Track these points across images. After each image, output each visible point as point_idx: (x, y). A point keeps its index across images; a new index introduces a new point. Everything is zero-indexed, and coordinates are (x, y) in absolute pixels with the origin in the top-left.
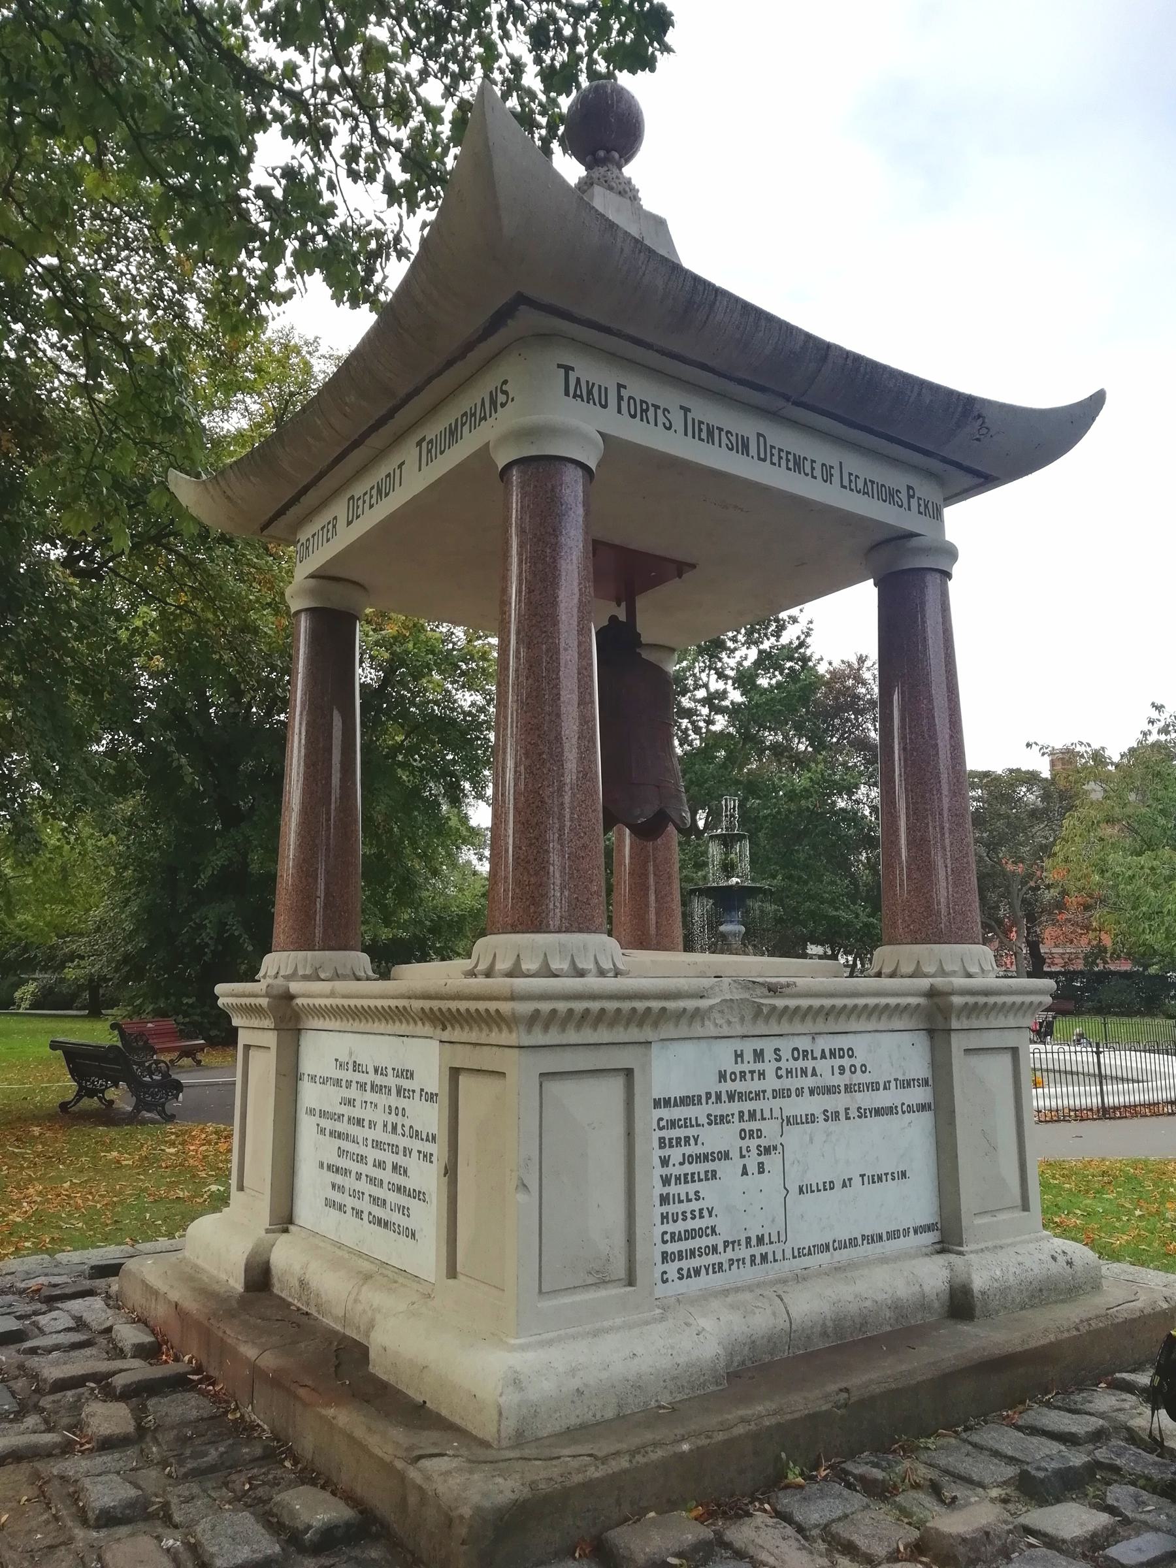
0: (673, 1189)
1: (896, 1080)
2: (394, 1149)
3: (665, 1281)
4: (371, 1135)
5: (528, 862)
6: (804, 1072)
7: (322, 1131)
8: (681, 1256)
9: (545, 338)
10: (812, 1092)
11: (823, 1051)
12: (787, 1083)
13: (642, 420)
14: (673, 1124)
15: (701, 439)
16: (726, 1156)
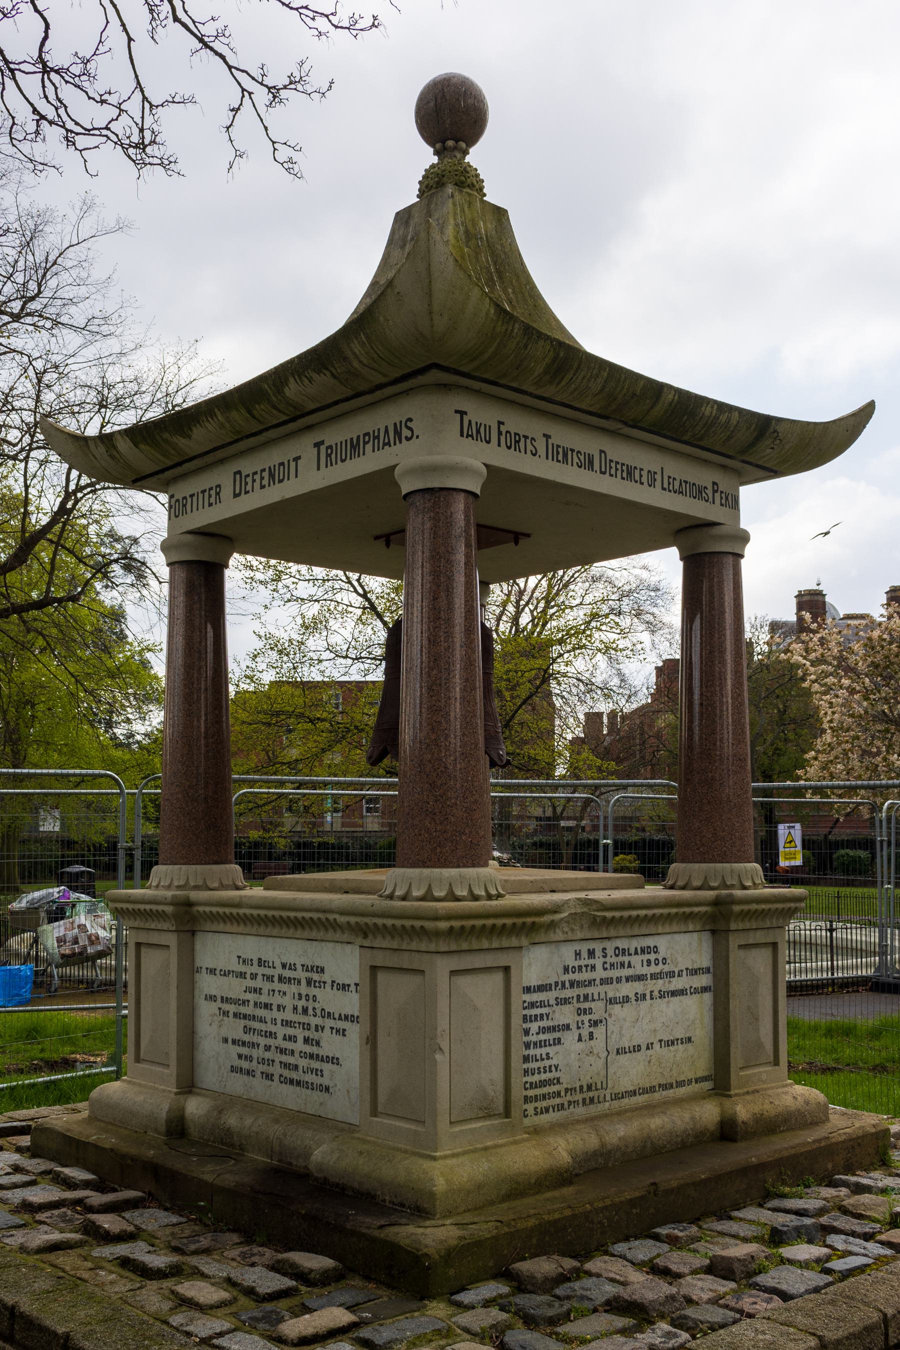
0: (532, 1052)
1: (687, 969)
2: (306, 1026)
3: (526, 1116)
4: (279, 1016)
5: (435, 814)
6: (622, 965)
7: (226, 1014)
8: (536, 1098)
9: (445, 387)
10: (627, 980)
11: (636, 949)
12: (615, 973)
13: (515, 450)
14: (532, 1005)
15: (558, 461)
16: (567, 1027)
